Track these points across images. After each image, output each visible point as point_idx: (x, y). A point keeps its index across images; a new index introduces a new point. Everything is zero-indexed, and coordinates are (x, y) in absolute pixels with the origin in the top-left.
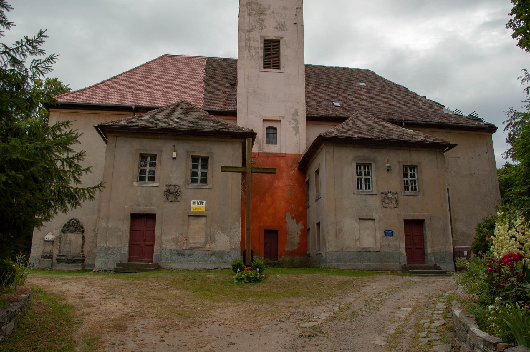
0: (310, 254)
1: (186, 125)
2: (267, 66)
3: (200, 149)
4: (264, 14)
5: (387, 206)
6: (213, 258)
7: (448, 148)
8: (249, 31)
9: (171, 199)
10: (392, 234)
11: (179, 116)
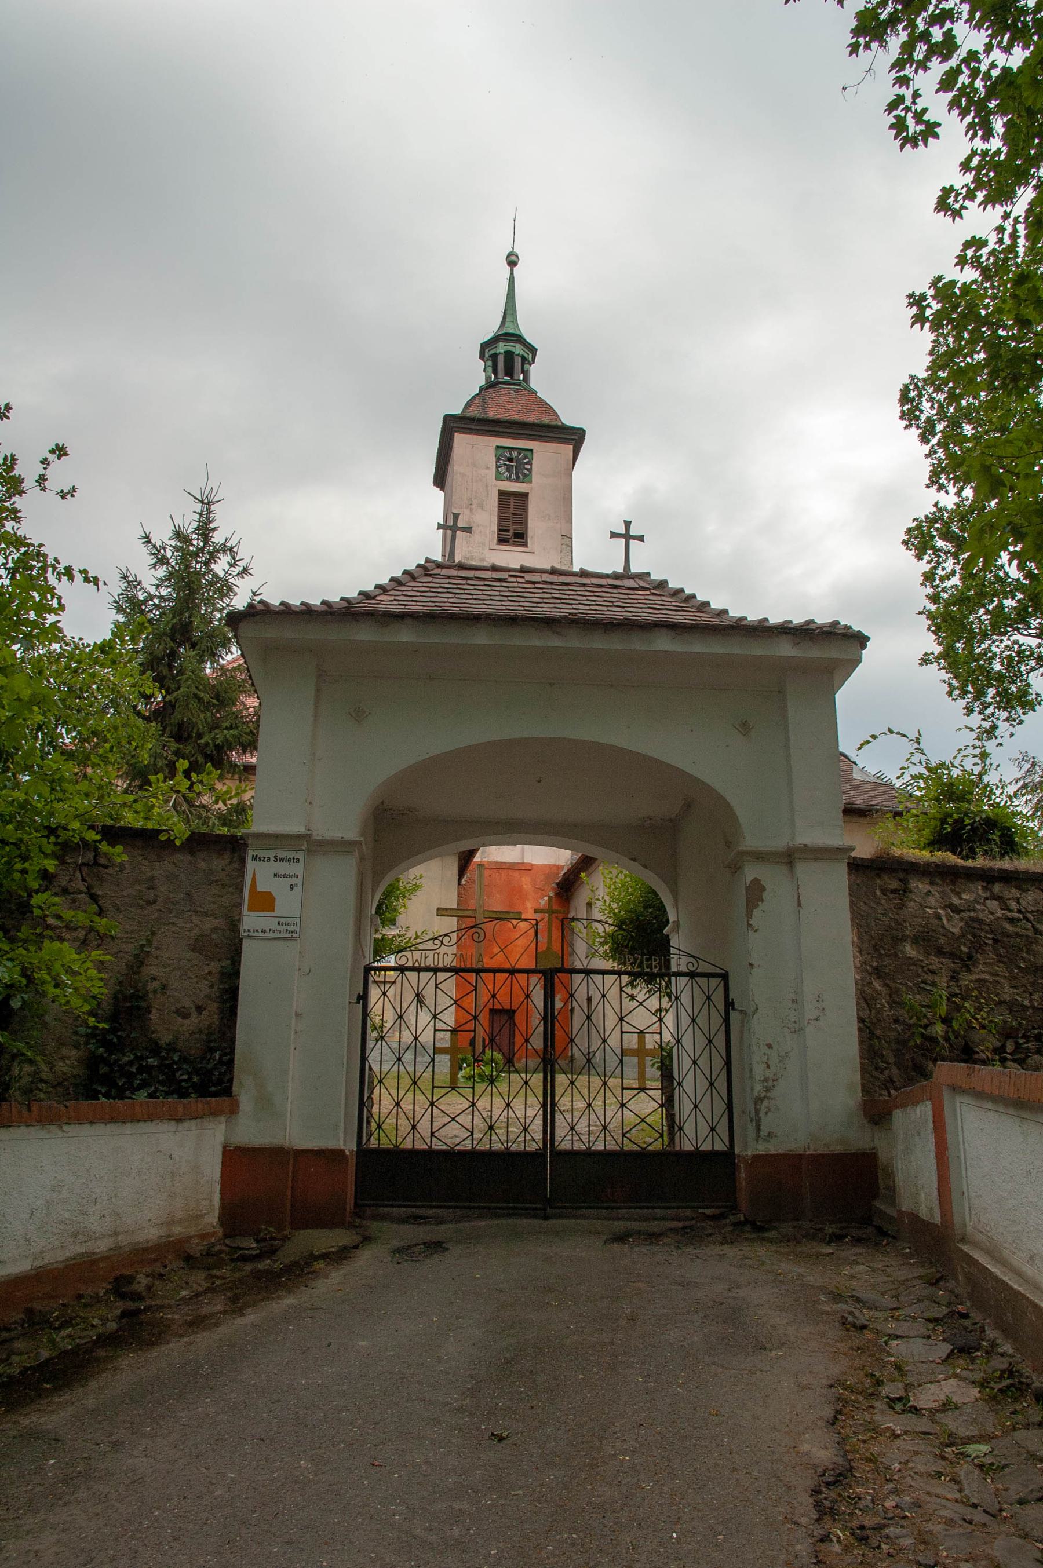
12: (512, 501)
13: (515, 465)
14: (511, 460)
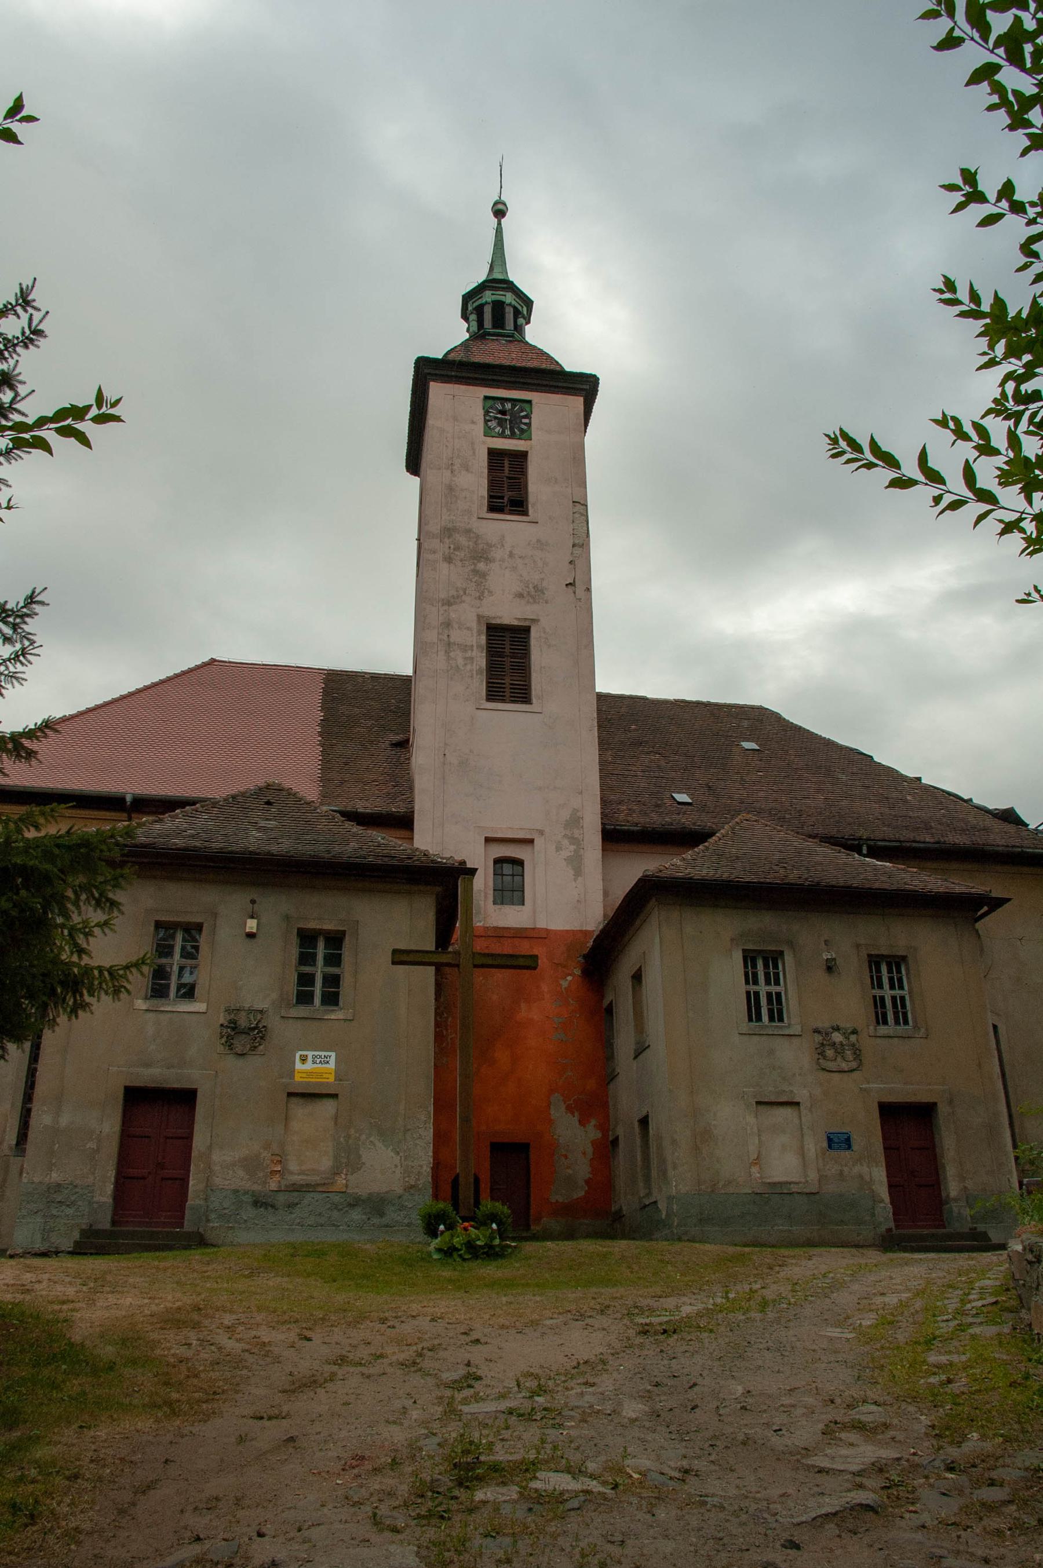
0: (621, 1209)
1: (284, 846)
2: (495, 693)
3: (323, 910)
4: (487, 559)
5: (831, 1065)
6: (356, 1215)
7: (986, 908)
8: (448, 603)
9: (239, 1049)
10: (847, 1143)
11: (262, 823)
12: (506, 463)
13: (511, 419)
14: (503, 412)
